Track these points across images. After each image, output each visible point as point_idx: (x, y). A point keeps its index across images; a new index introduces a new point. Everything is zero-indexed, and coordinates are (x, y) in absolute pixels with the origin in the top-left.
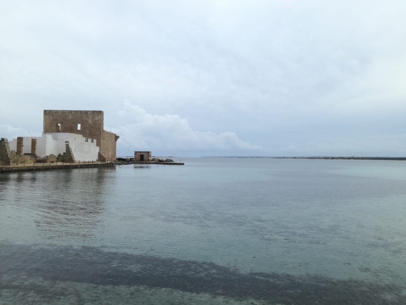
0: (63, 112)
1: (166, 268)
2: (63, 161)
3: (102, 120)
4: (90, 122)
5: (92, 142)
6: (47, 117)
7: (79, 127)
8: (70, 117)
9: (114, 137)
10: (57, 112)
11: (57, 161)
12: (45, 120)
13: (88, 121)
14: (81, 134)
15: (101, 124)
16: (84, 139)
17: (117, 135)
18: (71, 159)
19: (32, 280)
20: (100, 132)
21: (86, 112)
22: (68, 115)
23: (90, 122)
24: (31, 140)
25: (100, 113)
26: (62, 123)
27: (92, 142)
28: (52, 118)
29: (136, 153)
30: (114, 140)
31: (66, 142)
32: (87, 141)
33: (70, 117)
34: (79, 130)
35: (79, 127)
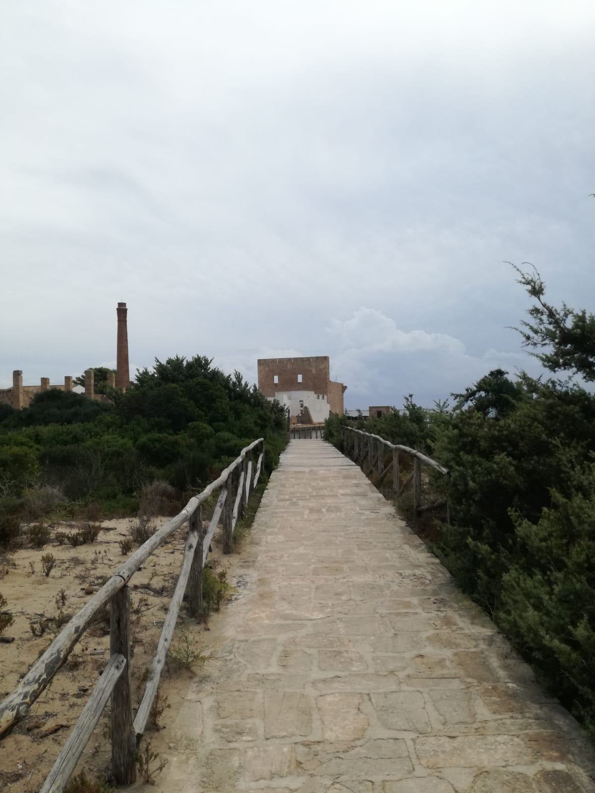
0: (127, 340)
1: (288, 622)
2: (302, 423)
3: (327, 368)
4: (314, 371)
5: (323, 398)
6: (262, 368)
7: (300, 378)
8: (289, 367)
9: (340, 388)
10: (273, 361)
11: (298, 423)
12: (260, 372)
13: (311, 371)
14: (312, 391)
15: (325, 372)
16: (316, 396)
17: (344, 385)
18: (309, 421)
19: (501, 548)
20: (327, 383)
21: (308, 359)
22: (287, 363)
23: (314, 371)
24: (64, 380)
25: (325, 359)
26: (279, 375)
27: (323, 398)
28: (267, 369)
29: (371, 408)
30: (341, 392)
31: (300, 401)
32: (318, 398)
33: (289, 367)
34: (300, 383)
35: (300, 378)
